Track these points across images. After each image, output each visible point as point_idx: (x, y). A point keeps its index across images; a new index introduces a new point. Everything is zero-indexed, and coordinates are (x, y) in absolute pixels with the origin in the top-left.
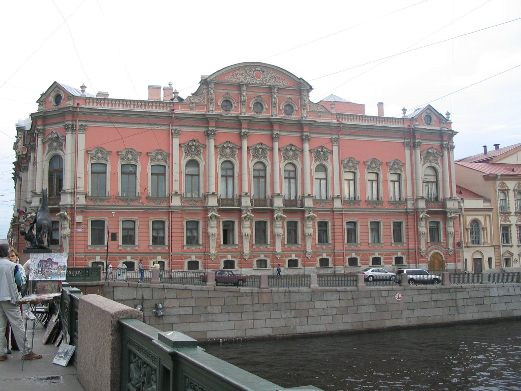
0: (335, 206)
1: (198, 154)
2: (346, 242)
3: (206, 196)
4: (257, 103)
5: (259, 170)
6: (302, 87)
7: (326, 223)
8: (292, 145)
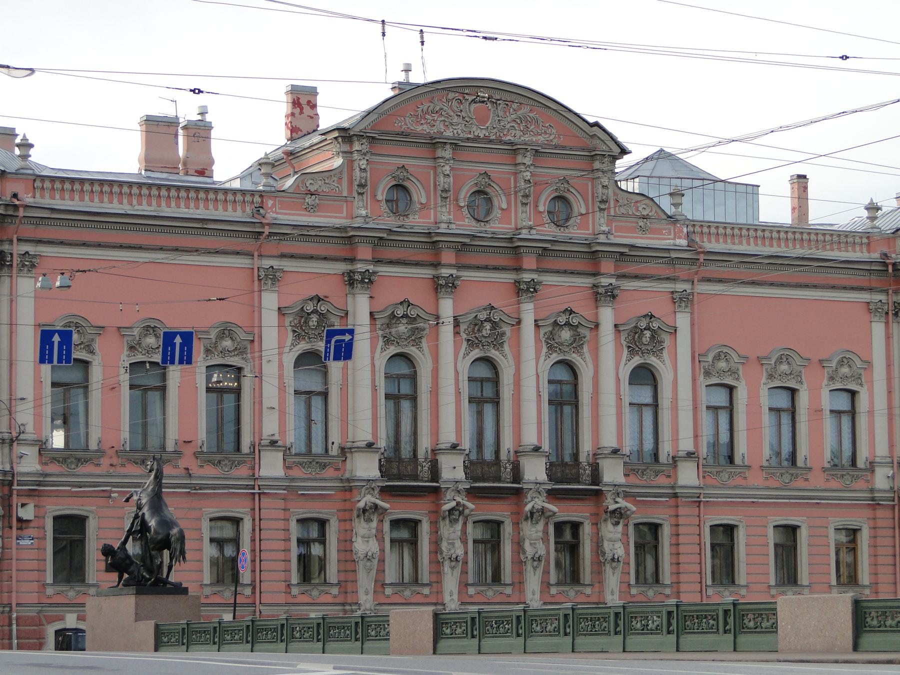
0: (681, 482)
1: (658, 352)
2: (709, 582)
3: (872, 467)
4: (479, 192)
5: (399, 377)
6: (596, 147)
7: (655, 528)
8: (571, 312)
